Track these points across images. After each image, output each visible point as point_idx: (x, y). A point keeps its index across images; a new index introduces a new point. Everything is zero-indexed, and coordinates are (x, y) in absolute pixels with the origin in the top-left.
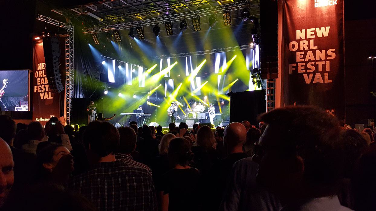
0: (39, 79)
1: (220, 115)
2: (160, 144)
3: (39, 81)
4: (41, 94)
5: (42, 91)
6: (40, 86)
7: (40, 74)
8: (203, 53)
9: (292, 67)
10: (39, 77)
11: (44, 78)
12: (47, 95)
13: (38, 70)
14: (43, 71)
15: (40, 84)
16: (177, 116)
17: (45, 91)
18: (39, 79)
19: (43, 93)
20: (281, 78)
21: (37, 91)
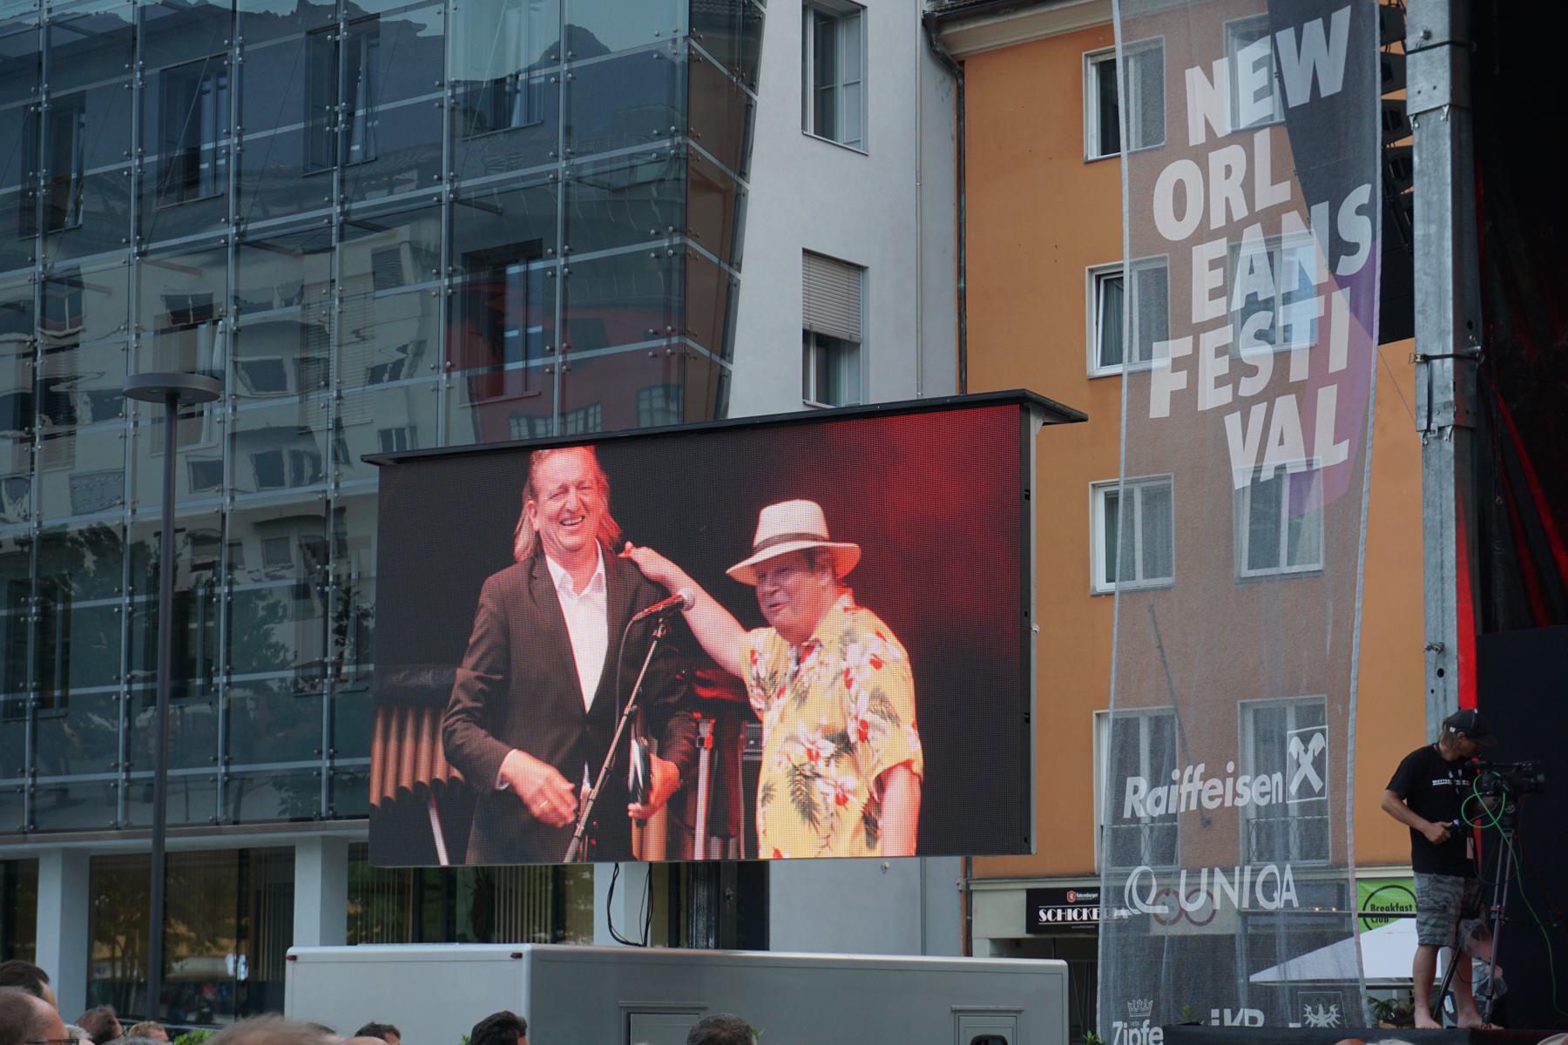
0: (1219, 248)
1: (438, 862)
2: (493, 677)
3: (1216, 278)
4: (1233, 422)
5: (1249, 387)
6: (1225, 335)
7: (1227, 195)
8: (388, 893)
9: (881, 670)
10: (1217, 221)
11: (1271, 221)
12: (1295, 435)
13: (1197, 136)
14: (1262, 140)
15: (1218, 308)
16: (1086, 1041)
17: (1280, 384)
18: (1219, 248)
19: (1258, 411)
20: (1032, 580)
21: (1184, 400)
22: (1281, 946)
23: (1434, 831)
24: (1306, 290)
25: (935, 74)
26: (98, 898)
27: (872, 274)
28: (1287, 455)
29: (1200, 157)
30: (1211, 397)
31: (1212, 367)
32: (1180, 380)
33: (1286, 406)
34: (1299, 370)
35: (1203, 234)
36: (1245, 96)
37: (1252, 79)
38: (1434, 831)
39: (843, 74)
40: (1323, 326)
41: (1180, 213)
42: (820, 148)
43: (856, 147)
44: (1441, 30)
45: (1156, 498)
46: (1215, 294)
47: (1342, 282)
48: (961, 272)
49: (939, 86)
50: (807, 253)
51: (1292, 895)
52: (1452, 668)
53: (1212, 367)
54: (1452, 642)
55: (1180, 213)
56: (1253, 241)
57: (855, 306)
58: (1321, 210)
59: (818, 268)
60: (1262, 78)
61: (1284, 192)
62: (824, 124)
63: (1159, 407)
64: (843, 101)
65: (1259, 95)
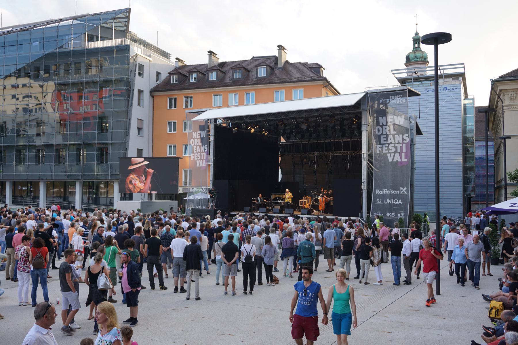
4: (197, 161)
5: (198, 159)
11: (200, 146)
14: (199, 139)
15: (196, 152)
17: (201, 159)
18: (196, 147)
19: (199, 161)
22: (195, 202)
23: (211, 195)
24: (203, 152)
25: (151, 97)
26: (329, 191)
27: (144, 121)
28: (201, 165)
29: (194, 139)
30: (196, 159)
31: (196, 157)
32: (193, 157)
33: (201, 161)
34: (202, 158)
35: (194, 146)
36: (198, 136)
37: (198, 135)
38: (211, 195)
39: (141, 98)
40: (204, 155)
41: (192, 143)
42: (139, 107)
43: (143, 107)
44: (213, 134)
45: (175, 146)
46: (195, 151)
47: (205, 152)
48: (153, 120)
49: (151, 99)
50: (138, 119)
51: (123, 233)
52: (212, 182)
53: (196, 157)
54: (212, 180)
55: (192, 143)
56: (198, 147)
57: (142, 124)
58: (203, 146)
59: (138, 120)
60: (199, 134)
61: (201, 144)
62: (139, 104)
63: (192, 159)
64: (141, 101)
65: (199, 136)
